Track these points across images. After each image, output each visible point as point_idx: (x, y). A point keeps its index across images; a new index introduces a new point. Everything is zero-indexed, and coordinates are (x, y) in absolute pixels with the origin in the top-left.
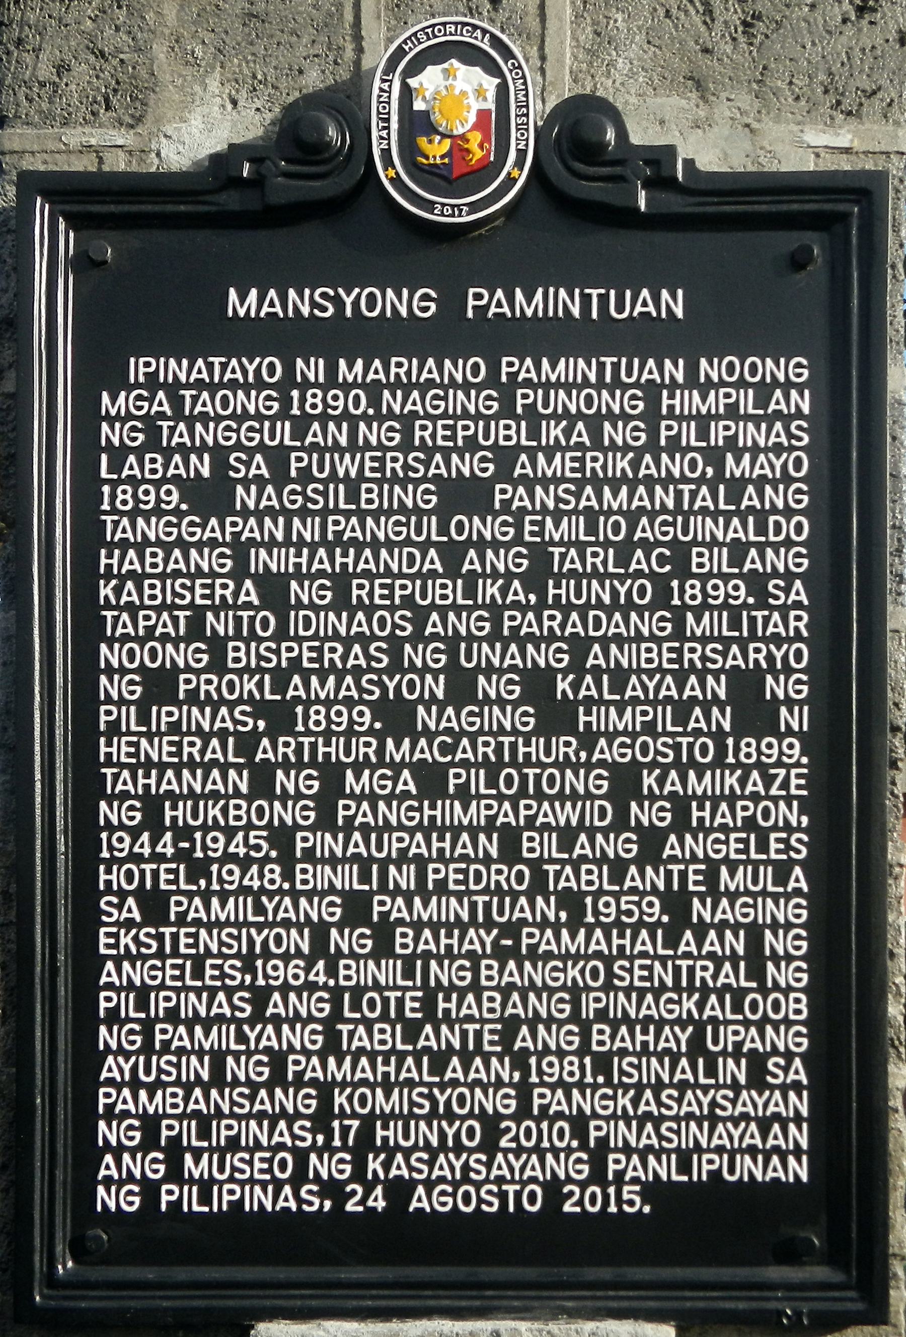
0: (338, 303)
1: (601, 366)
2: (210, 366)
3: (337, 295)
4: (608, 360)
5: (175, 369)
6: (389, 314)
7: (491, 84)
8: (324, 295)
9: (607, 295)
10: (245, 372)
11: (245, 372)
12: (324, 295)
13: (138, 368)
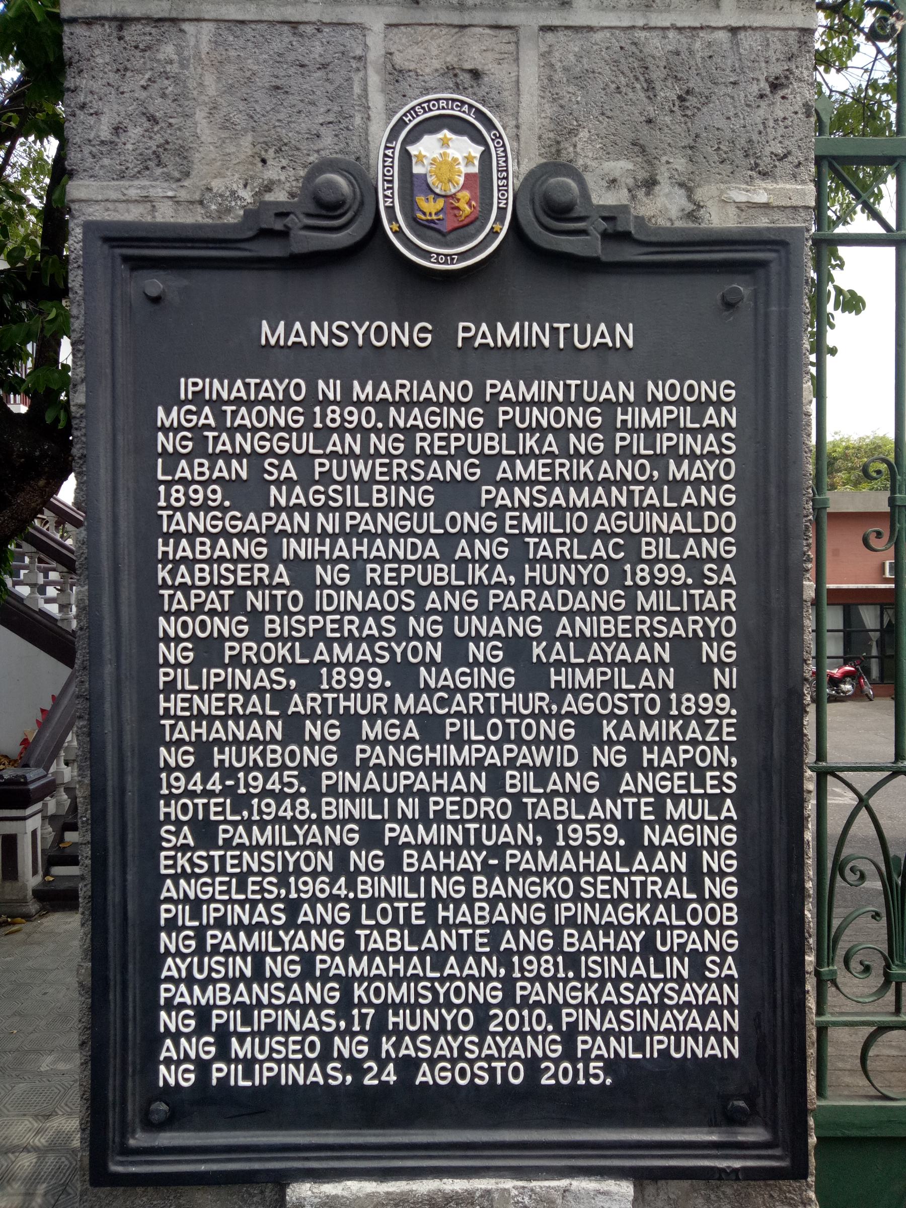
0: (351, 332)
1: (567, 387)
2: (247, 386)
3: (351, 327)
4: (573, 383)
5: (218, 388)
6: (394, 343)
7: (476, 150)
8: (340, 328)
9: (572, 328)
12: (340, 328)
13: (187, 387)
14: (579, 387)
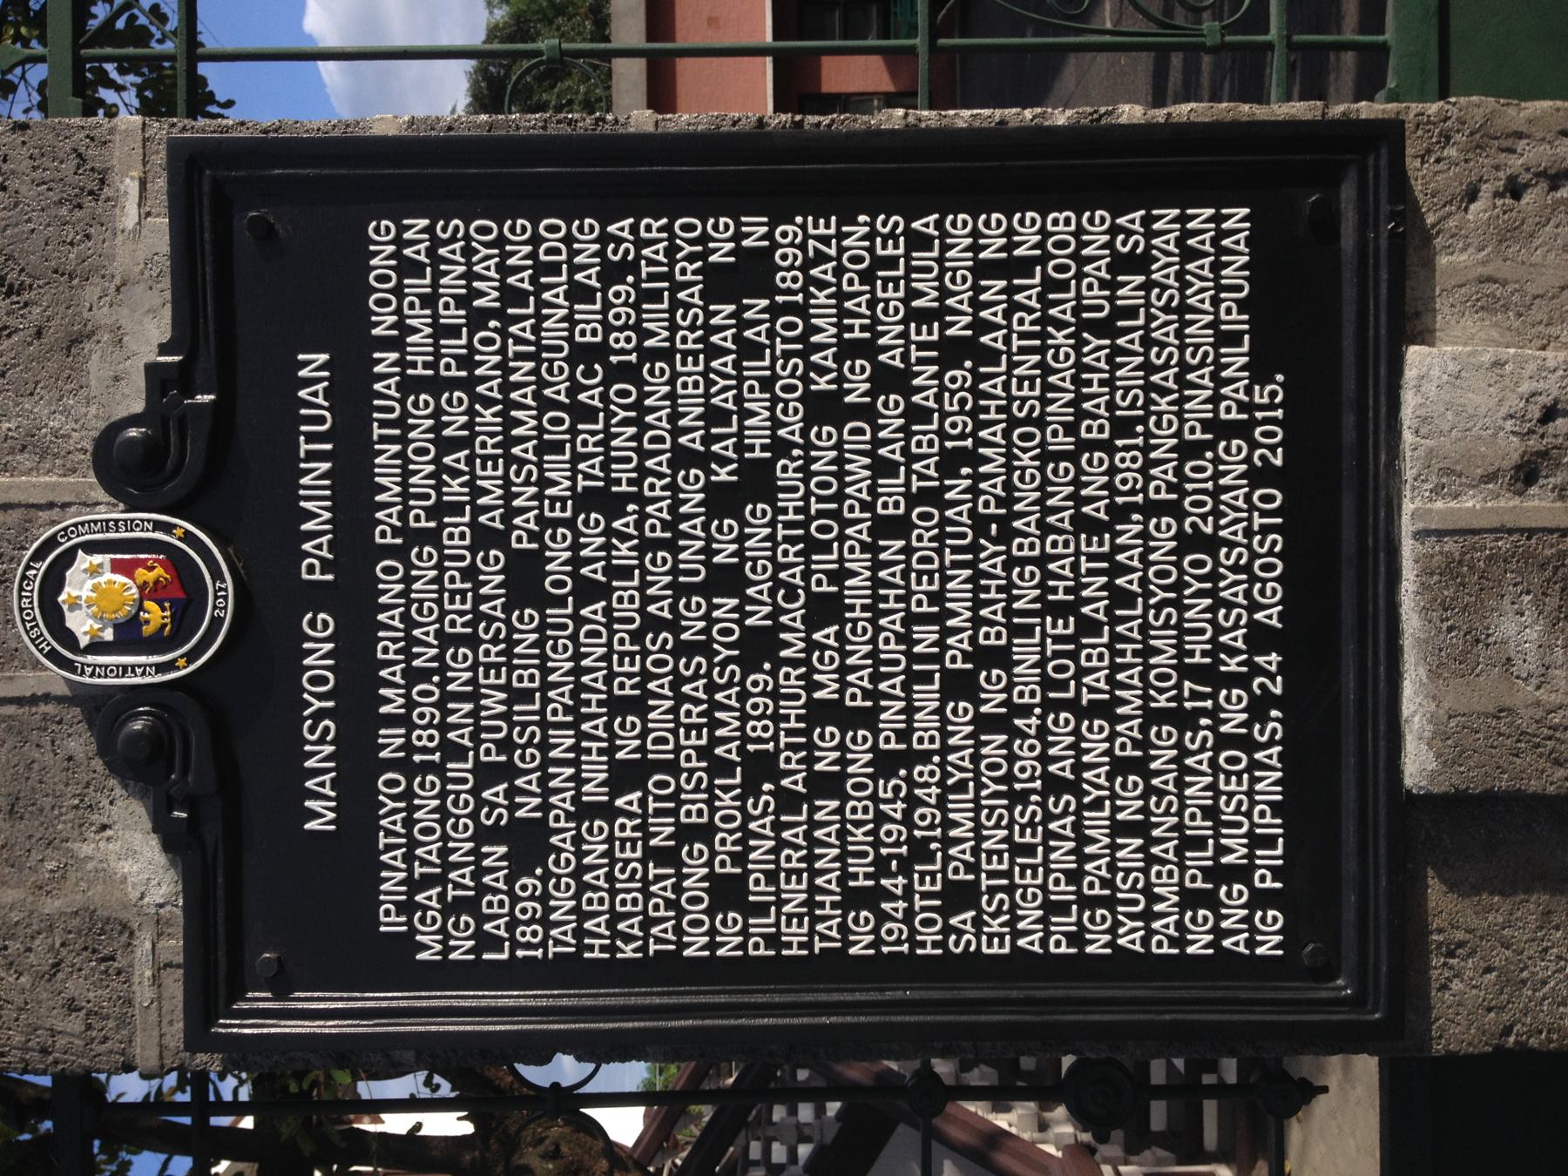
0: (319, 715)
3: (310, 716)
5: (392, 884)
8: (312, 730)
9: (306, 434)
10: (394, 811)
11: (394, 811)
12: (312, 730)
13: (391, 923)
14: (311, 438)
